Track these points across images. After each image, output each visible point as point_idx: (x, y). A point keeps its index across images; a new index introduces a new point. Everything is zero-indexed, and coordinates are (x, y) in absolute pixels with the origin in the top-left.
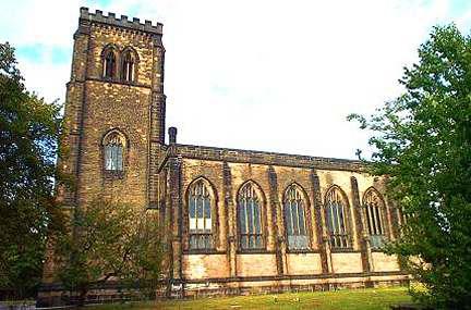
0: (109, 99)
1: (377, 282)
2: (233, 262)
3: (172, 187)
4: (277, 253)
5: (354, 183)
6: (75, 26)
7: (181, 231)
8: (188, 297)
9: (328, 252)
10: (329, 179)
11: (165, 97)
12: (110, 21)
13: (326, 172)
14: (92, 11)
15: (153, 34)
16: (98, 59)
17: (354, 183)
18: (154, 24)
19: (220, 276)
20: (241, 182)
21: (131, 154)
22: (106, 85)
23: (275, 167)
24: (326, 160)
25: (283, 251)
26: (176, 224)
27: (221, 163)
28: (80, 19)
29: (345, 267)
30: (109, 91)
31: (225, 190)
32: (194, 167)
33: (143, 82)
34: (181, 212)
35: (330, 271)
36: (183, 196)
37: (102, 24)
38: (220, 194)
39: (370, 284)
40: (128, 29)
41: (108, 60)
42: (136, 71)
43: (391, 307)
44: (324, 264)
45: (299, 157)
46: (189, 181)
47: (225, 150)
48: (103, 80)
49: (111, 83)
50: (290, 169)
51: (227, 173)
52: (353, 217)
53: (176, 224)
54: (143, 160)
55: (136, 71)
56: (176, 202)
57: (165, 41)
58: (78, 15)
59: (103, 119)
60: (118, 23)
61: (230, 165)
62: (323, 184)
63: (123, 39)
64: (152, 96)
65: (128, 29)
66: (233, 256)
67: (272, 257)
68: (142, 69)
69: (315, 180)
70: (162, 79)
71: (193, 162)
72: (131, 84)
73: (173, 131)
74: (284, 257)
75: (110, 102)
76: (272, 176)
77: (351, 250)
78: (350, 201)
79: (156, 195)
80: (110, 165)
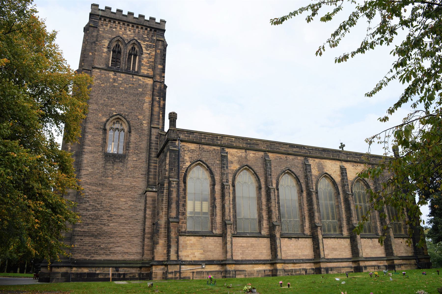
0: (114, 86)
1: (366, 267)
2: (229, 245)
3: (171, 169)
4: (272, 237)
5: (343, 171)
6: (86, 20)
7: (178, 213)
8: (184, 278)
9: (320, 237)
10: (321, 168)
11: (165, 87)
12: (117, 17)
13: (317, 160)
14: (102, 7)
15: (156, 30)
16: (105, 50)
17: (343, 171)
18: (158, 21)
19: (196, 259)
20: (238, 166)
21: (132, 139)
22: (111, 74)
23: (270, 155)
24: (317, 149)
25: (278, 235)
26: (174, 206)
27: (219, 148)
28: (91, 14)
29: (335, 253)
30: (114, 79)
31: (222, 174)
32: (193, 151)
33: (146, 72)
34: (178, 196)
35: (322, 256)
36: (181, 179)
37: (110, 19)
38: (217, 178)
39: (358, 269)
40: (133, 24)
41: (114, 51)
42: (140, 62)
43: (439, 292)
44: (274, 249)
45: (292, 146)
46: (188, 164)
47: (223, 136)
48: (108, 69)
49: (115, 71)
50: (283, 156)
51: (224, 158)
52: (342, 204)
53: (174, 206)
54: (144, 145)
55: (140, 62)
56: (174, 185)
57: (167, 36)
58: (90, 11)
59: (106, 106)
60: (125, 19)
61: (227, 150)
62: (315, 172)
63: (129, 33)
64: (154, 86)
65: (133, 24)
66: (229, 239)
67: (219, 240)
68: (145, 60)
69: (307, 168)
70: (163, 70)
71: (192, 146)
72: (137, 74)
73: (173, 117)
74: (278, 241)
75: (114, 89)
76: (266, 163)
77: (341, 237)
78: (340, 188)
79: (155, 179)
80: (112, 149)
